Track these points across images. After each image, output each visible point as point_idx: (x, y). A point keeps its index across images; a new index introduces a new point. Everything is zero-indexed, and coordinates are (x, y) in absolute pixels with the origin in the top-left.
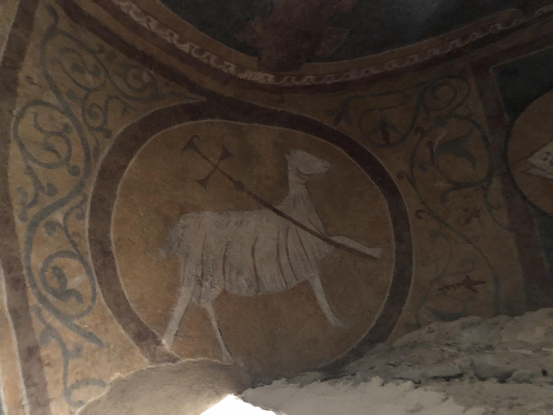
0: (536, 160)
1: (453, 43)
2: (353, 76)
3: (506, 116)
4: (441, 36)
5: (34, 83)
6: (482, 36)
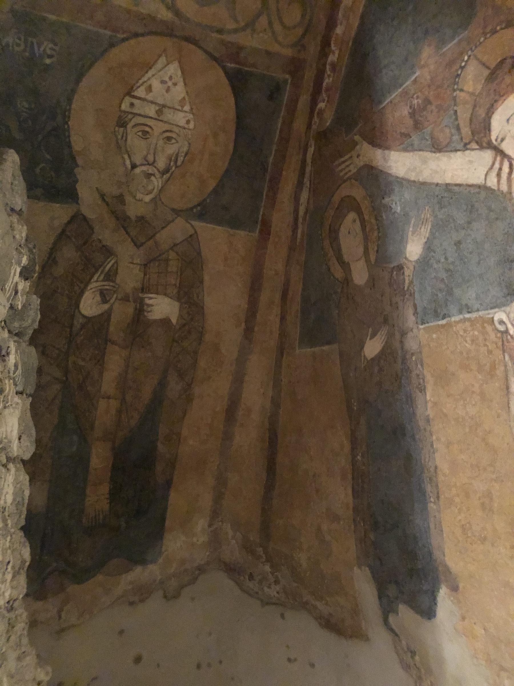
0: (174, 69)
3: (233, 65)
4: (350, 44)
5: (428, 58)
6: (324, 84)
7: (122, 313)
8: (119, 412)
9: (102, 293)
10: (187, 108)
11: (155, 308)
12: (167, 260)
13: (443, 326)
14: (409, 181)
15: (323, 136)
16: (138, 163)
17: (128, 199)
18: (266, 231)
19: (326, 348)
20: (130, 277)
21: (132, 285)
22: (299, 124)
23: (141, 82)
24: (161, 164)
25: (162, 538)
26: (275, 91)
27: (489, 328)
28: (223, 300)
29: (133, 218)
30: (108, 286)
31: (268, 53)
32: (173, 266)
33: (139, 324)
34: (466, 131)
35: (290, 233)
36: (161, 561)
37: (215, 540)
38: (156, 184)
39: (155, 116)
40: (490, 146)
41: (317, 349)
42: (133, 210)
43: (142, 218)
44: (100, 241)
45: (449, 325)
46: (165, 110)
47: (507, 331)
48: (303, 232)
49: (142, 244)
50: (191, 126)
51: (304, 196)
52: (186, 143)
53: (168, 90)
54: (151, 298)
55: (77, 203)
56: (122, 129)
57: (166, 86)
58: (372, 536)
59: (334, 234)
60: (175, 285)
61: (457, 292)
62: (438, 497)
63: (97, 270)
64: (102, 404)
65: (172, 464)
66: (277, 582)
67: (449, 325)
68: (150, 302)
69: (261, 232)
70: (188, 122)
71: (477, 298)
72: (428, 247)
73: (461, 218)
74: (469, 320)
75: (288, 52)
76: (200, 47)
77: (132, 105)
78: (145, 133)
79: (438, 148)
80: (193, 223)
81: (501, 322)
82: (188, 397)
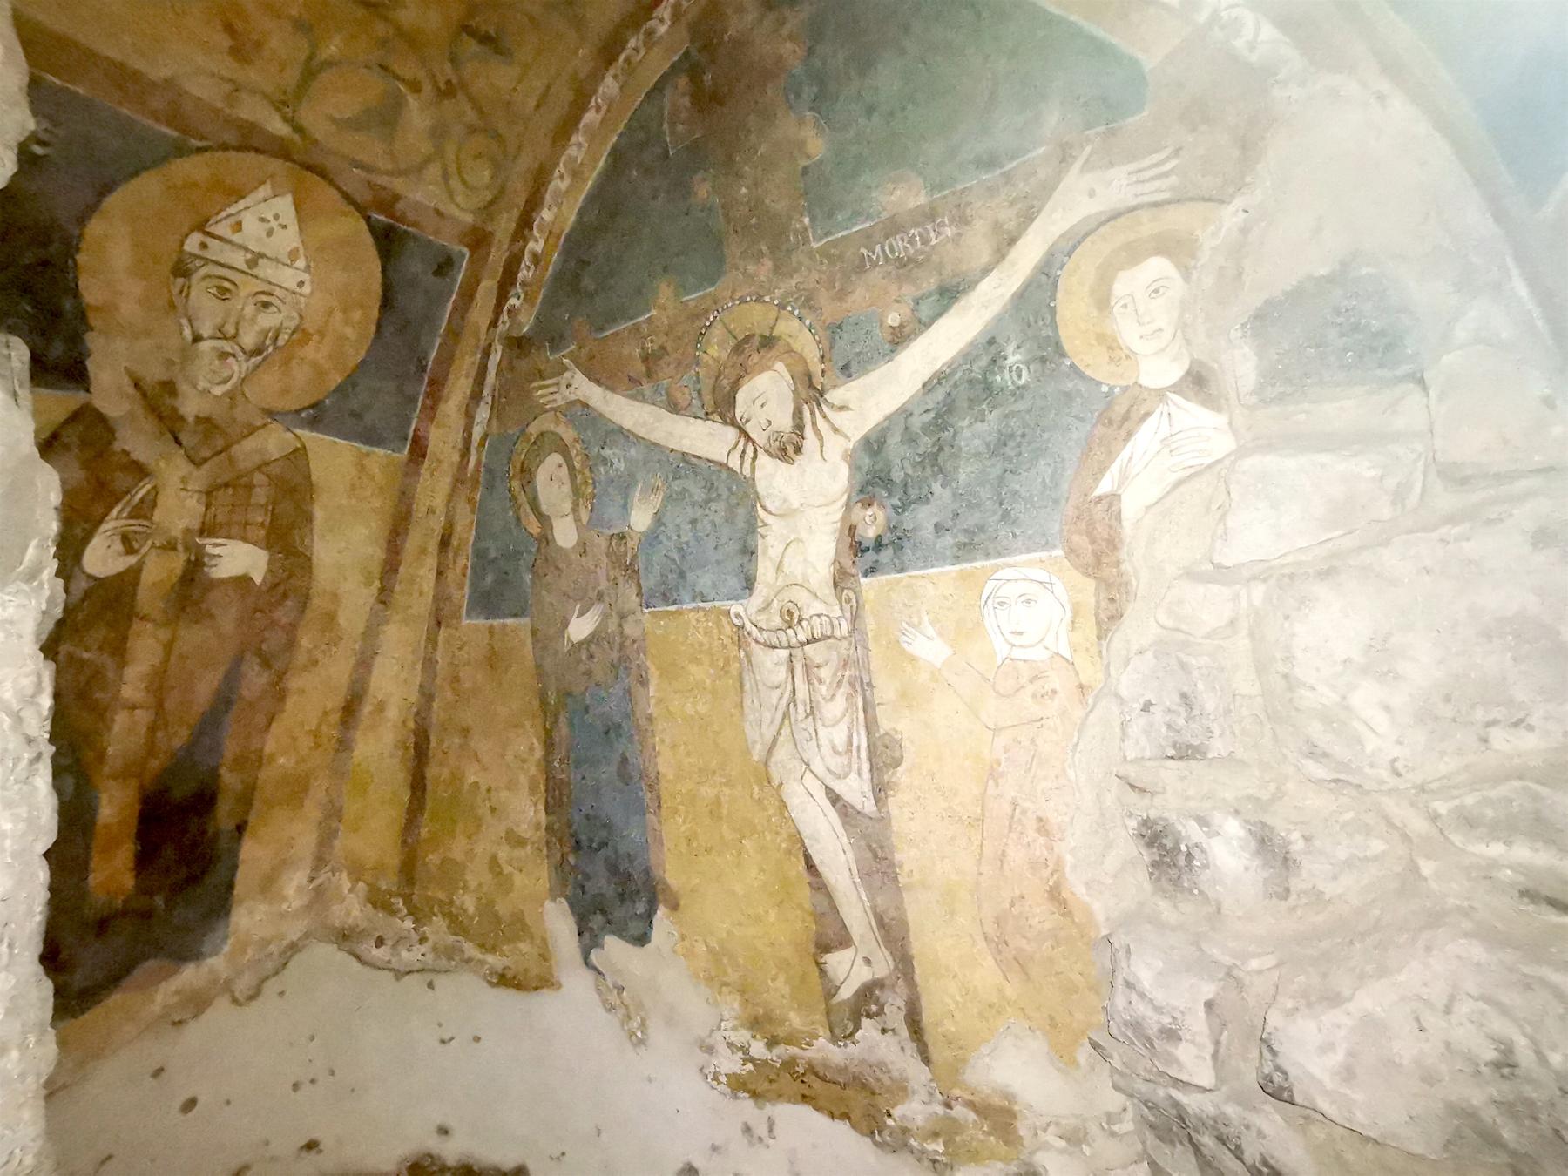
1: (542, 242)
2: (609, 86)
3: (382, 218)
7: (159, 571)
8: (152, 729)
9: (126, 539)
10: (301, 263)
11: (224, 560)
12: (250, 487)
13: (672, 613)
14: (637, 437)
15: (518, 345)
16: (205, 335)
17: (183, 387)
18: (419, 450)
19: (510, 621)
20: (179, 508)
21: (182, 525)
22: (480, 314)
23: (224, 214)
24: (249, 340)
25: (227, 914)
26: (445, 266)
27: (724, 620)
28: (342, 549)
29: (191, 419)
30: (136, 525)
31: (438, 212)
32: (261, 495)
33: (193, 583)
34: (708, 399)
35: (456, 457)
36: (226, 949)
37: (319, 897)
38: (236, 368)
39: (245, 268)
40: (733, 423)
41: (496, 622)
42: (190, 406)
43: (208, 420)
44: (127, 453)
45: (679, 613)
46: (261, 261)
47: (743, 627)
48: (479, 463)
49: (205, 460)
50: (307, 289)
51: (483, 413)
52: (295, 314)
53: (270, 233)
54: (217, 545)
55: (88, 391)
56: (180, 280)
57: (267, 226)
58: (572, 859)
59: (527, 474)
60: (262, 524)
61: (690, 576)
62: (659, 806)
63: (118, 501)
64: (121, 720)
65: (246, 799)
66: (423, 940)
67: (679, 613)
68: (217, 551)
69: (412, 451)
70: (301, 284)
71: (714, 586)
72: (658, 519)
73: (698, 493)
74: (704, 609)
75: (469, 218)
76: (332, 183)
77: (204, 246)
78: (225, 290)
79: (674, 408)
80: (298, 432)
81: (738, 616)
82: (279, 694)
